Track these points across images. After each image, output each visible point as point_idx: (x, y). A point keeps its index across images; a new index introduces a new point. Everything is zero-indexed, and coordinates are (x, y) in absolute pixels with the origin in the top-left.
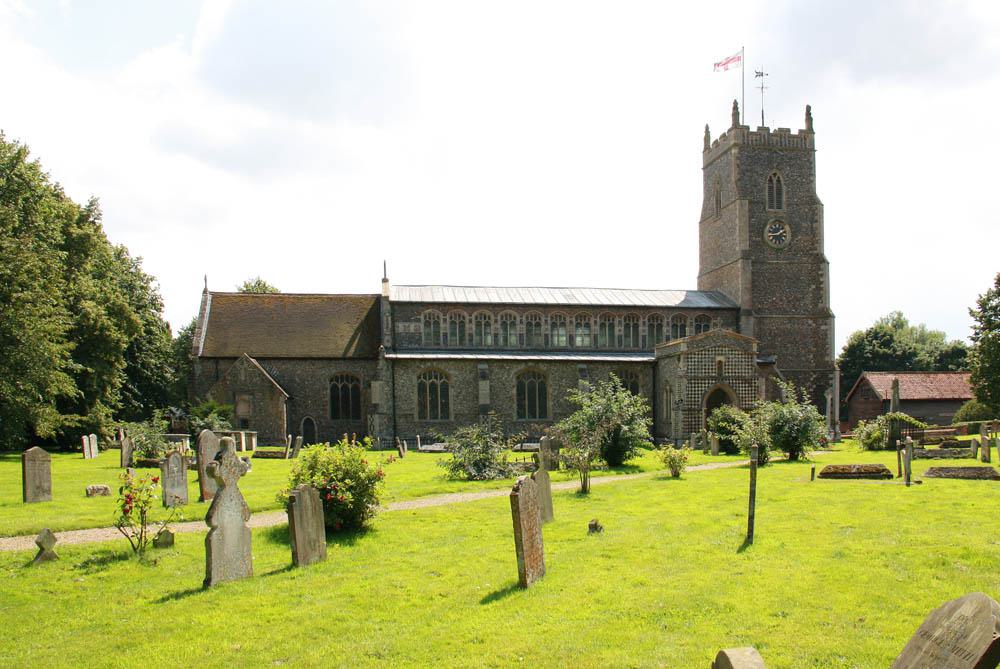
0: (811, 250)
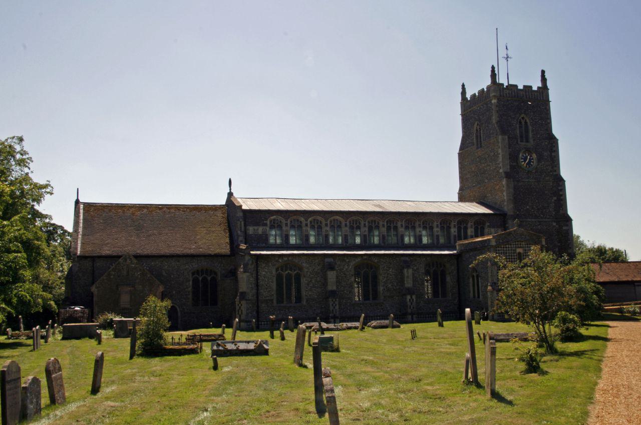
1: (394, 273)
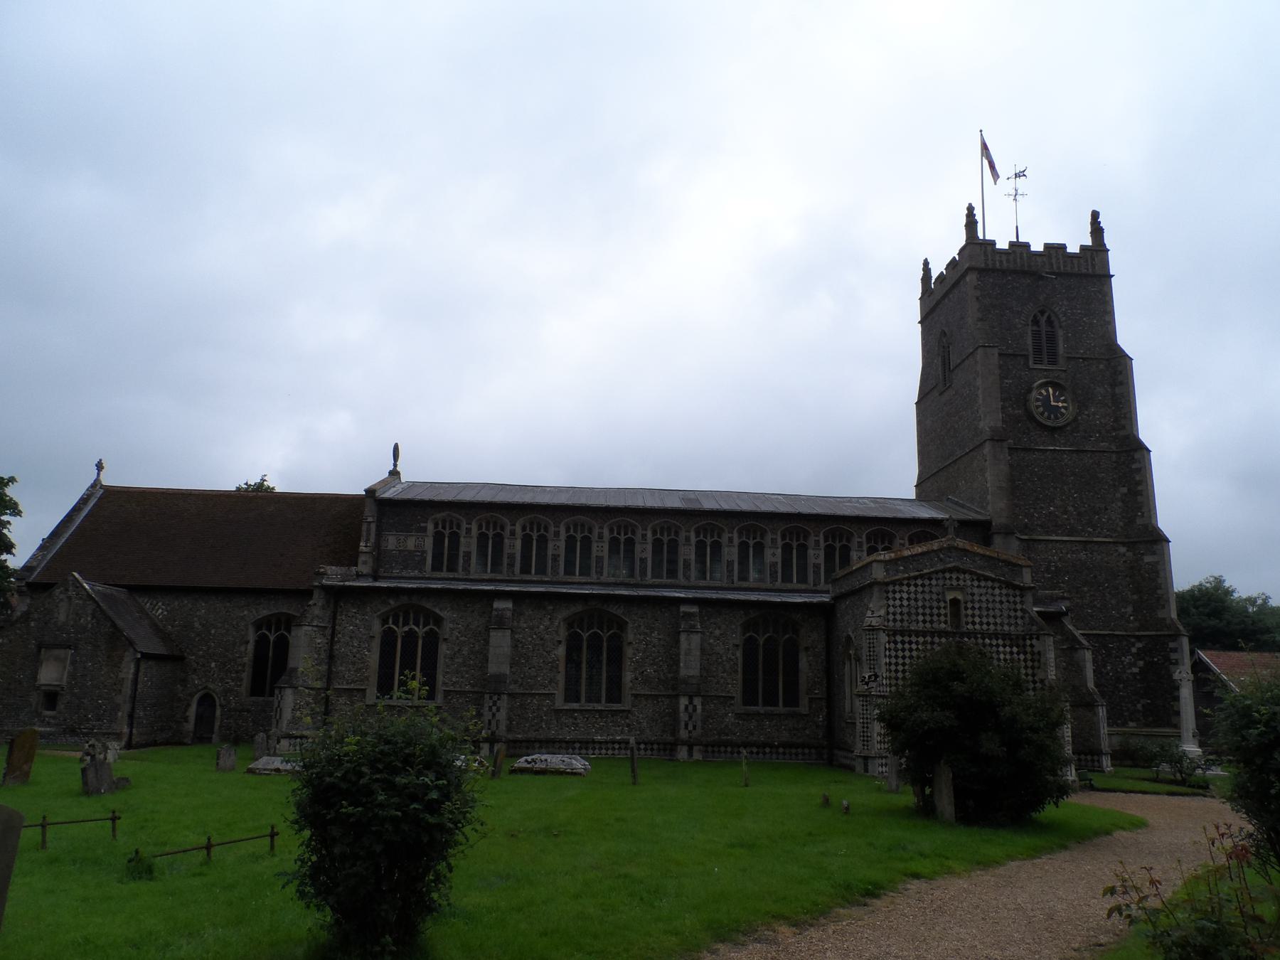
0: (1114, 429)
1: (662, 642)
